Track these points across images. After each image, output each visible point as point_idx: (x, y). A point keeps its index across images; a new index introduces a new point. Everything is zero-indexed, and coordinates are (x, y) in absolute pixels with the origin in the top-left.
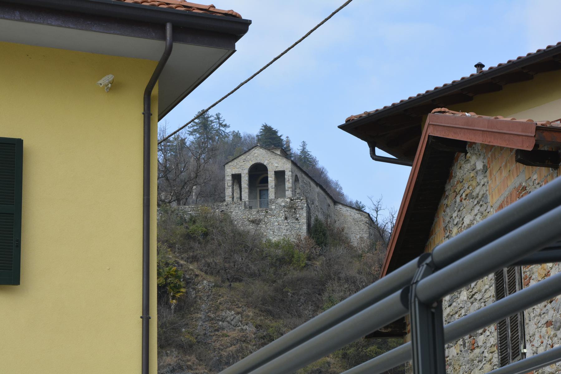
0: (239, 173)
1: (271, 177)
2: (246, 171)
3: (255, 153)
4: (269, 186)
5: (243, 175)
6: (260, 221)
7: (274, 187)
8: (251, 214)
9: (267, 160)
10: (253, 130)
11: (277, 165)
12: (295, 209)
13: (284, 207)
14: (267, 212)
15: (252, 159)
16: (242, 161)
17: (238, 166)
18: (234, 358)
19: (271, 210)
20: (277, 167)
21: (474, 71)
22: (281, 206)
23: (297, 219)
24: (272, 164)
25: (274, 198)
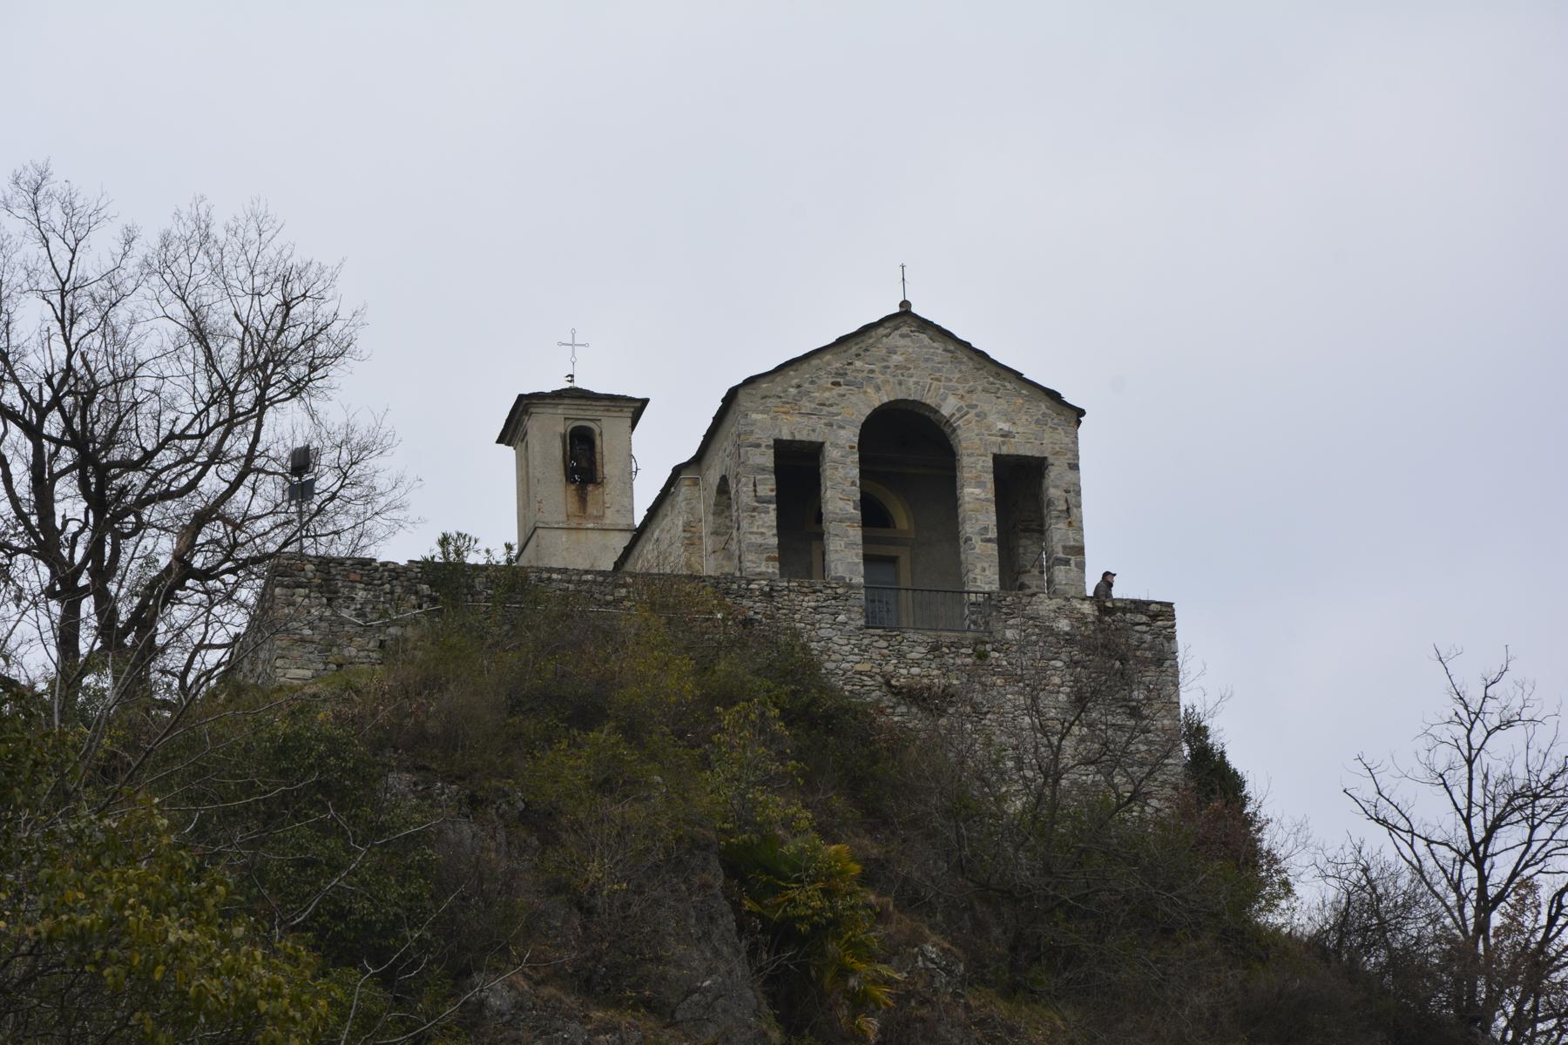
0: (813, 438)
1: (980, 484)
2: (850, 436)
3: (892, 351)
4: (969, 529)
5: (832, 453)
6: (947, 695)
7: (993, 534)
8: (901, 656)
9: (954, 391)
10: (509, 452)
11: (1006, 427)
12: (1123, 660)
13: (1069, 639)
14: (983, 656)
15: (880, 378)
16: (826, 381)
17: (807, 405)
18: (437, 1003)
19: (1002, 646)
20: (1006, 435)
21: (436, 553)
22: (1056, 634)
23: (1135, 713)
24: (981, 416)
25: (995, 587)
